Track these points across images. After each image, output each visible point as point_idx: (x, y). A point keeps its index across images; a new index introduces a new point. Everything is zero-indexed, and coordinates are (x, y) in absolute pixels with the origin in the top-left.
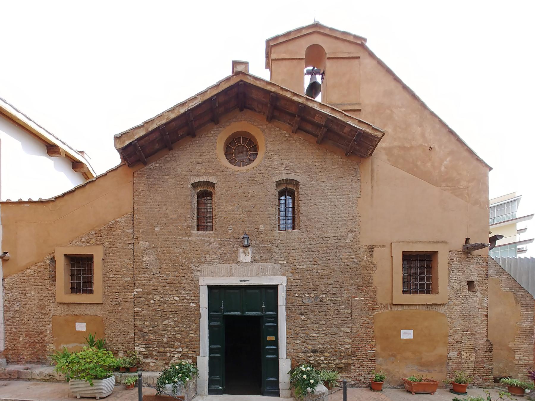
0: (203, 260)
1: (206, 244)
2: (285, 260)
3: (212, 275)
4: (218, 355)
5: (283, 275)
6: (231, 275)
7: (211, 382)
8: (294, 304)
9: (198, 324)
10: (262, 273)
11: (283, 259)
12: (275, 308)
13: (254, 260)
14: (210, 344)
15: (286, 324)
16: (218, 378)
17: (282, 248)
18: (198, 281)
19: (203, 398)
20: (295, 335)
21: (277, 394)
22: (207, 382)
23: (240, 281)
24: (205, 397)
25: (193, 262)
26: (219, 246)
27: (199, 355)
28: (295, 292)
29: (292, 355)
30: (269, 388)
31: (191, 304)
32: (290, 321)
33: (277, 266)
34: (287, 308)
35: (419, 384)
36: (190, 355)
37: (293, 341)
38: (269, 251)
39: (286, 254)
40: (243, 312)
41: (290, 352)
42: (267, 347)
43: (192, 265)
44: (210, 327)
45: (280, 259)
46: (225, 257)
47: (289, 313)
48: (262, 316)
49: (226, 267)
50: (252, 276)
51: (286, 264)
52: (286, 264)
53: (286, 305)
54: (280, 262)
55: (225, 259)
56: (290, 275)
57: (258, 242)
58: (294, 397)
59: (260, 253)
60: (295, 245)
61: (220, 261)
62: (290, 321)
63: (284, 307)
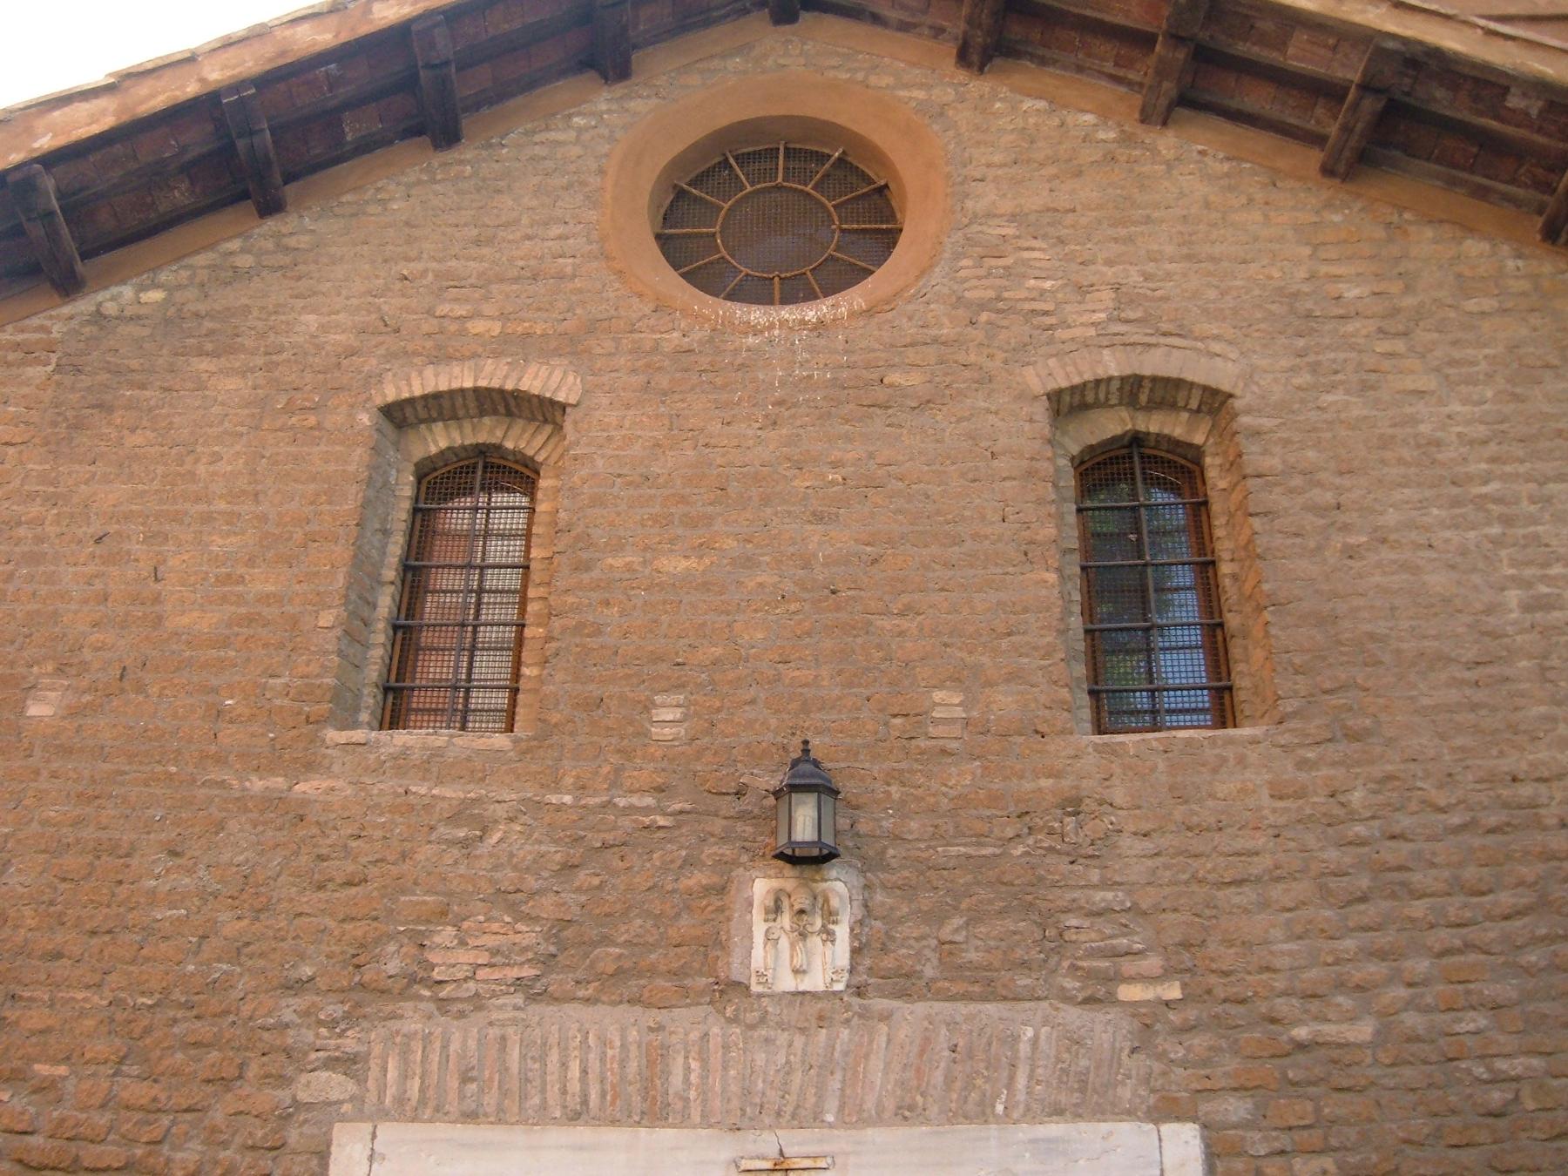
5: (1165, 1110)
11: (1153, 963)
13: (880, 973)
17: (1137, 871)
25: (297, 987)
26: (556, 854)
33: (1105, 1030)
43: (288, 1010)
46: (606, 940)
51: (1192, 1014)
52: (1192, 1014)
54: (1130, 992)
56: (1236, 1108)
59: (936, 917)
60: (1260, 841)
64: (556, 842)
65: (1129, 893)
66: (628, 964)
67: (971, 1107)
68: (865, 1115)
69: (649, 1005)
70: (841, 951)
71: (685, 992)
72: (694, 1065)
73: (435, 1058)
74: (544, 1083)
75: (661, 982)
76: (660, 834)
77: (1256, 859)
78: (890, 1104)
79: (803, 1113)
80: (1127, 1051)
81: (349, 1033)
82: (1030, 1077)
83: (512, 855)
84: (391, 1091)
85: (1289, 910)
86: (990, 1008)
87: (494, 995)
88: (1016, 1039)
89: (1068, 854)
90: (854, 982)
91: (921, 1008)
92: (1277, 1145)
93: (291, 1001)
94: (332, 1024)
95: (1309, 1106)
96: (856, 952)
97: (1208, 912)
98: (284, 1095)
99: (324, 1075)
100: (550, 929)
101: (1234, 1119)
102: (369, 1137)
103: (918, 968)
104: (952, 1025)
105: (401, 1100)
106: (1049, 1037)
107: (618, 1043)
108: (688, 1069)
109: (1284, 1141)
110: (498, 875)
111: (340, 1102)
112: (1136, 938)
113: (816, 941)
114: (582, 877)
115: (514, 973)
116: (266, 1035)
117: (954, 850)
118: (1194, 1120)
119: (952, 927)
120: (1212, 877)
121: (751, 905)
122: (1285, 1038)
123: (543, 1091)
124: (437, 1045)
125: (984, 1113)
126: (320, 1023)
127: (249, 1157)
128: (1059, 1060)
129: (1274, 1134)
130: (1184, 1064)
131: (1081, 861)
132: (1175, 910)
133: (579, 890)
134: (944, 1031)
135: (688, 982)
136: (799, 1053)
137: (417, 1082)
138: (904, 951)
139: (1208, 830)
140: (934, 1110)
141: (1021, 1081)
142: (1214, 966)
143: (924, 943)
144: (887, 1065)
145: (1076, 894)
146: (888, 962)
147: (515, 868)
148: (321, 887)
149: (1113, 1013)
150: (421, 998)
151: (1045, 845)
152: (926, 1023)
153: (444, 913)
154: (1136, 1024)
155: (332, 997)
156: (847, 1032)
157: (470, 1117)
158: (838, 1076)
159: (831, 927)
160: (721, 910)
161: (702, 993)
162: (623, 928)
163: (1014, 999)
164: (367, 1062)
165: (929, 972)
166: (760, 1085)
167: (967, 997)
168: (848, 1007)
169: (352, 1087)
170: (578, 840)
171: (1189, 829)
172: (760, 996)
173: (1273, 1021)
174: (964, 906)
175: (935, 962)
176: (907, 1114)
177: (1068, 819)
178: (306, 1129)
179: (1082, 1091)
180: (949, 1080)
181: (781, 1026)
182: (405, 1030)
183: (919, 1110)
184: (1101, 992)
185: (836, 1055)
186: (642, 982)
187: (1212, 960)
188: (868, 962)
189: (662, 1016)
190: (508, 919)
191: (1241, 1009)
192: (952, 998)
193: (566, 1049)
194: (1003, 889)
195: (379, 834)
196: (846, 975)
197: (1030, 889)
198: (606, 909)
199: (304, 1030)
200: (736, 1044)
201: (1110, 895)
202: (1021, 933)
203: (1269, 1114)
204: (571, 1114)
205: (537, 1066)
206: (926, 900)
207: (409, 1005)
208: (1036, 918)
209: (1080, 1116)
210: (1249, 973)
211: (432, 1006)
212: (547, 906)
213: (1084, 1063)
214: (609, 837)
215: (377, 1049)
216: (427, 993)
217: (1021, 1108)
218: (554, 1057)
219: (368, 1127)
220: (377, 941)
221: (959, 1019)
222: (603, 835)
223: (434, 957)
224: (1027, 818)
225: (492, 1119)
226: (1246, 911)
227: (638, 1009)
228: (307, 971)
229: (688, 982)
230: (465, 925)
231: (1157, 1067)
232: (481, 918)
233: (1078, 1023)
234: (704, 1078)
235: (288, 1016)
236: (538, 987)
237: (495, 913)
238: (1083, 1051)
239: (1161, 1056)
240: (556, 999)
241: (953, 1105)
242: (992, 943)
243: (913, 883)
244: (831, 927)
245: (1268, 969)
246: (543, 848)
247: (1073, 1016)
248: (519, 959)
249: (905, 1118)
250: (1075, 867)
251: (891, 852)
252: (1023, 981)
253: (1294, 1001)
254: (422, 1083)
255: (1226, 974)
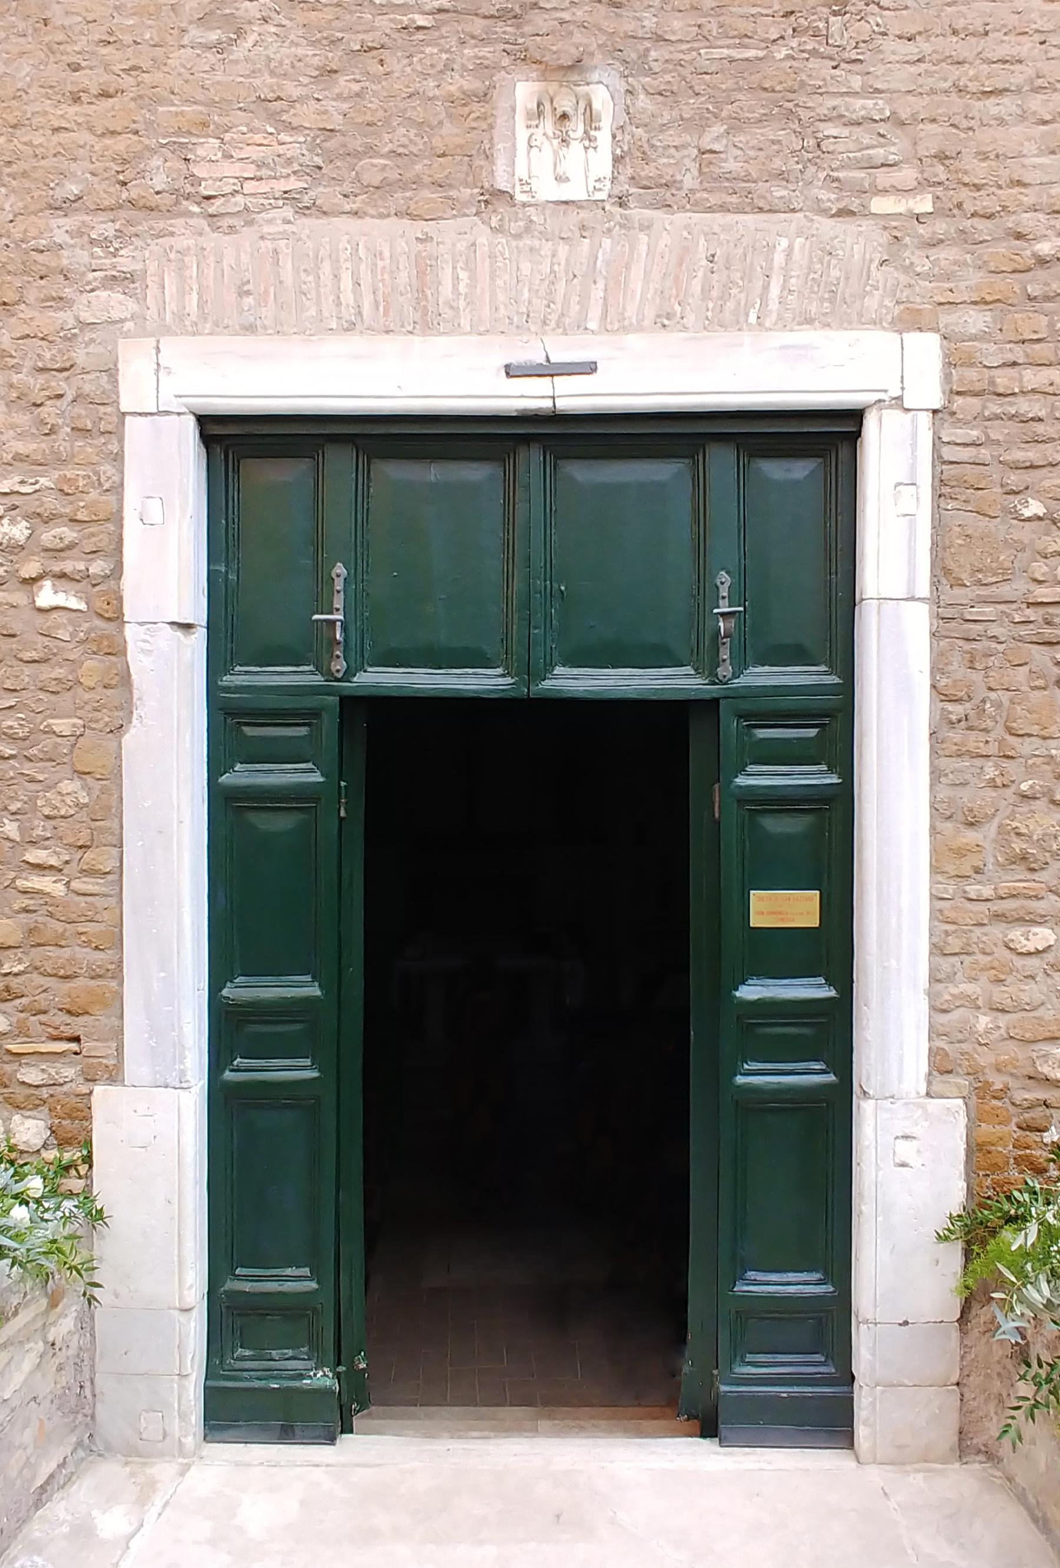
0: (159, 175)
1: (195, 34)
2: (925, 184)
3: (246, 314)
4: (300, 1070)
5: (910, 320)
6: (427, 320)
7: (231, 1320)
8: (1005, 591)
9: (107, 780)
10: (726, 309)
11: (907, 175)
12: (831, 628)
13: (642, 183)
14: (223, 963)
15: (936, 775)
16: (296, 1281)
17: (900, 78)
18: (112, 372)
19: (147, 1491)
20: (1016, 880)
21: (827, 1420)
22: (194, 1330)
23: (510, 372)
24: (164, 1471)
25: (63, 207)
26: (314, 57)
27: (114, 1075)
28: (1014, 479)
29: (985, 1059)
30: (755, 1373)
31: (47, 595)
32: (974, 742)
33: (859, 242)
34: (950, 627)
35: (345, 647)
36: (31, 1075)
37: (996, 931)
38: (785, 104)
39: (932, 138)
40: (531, 672)
41: (967, 1033)
42: (750, 992)
43: (60, 228)
44: (227, 808)
45: (883, 178)
46: (370, 151)
47: (957, 667)
48: (711, 705)
49: (371, 244)
50: (616, 324)
51: (941, 227)
52: (941, 227)
53: (935, 600)
54: (880, 205)
55: (373, 169)
56: (976, 320)
57: (678, 26)
58: (990, 1456)
59: (698, 124)
60: (1026, 47)
61: (324, 194)
62: (974, 742)
63: (918, 620)
64: (313, 44)
65: (889, 101)
66: (393, 175)
67: (727, 315)
68: (626, 323)
69: (413, 217)
70: (602, 162)
71: (453, 203)
72: (463, 275)
73: (210, 273)
74: (319, 296)
75: (426, 194)
76: (420, 36)
77: (1018, 67)
78: (650, 314)
79: (567, 321)
80: (876, 263)
81: (122, 252)
82: (783, 288)
83: (269, 60)
84: (171, 307)
85: (1045, 123)
86: (750, 219)
87: (263, 209)
88: (771, 248)
89: (832, 59)
90: (616, 192)
91: (681, 218)
92: (1010, 357)
93: (62, 221)
94: (104, 242)
95: (1044, 320)
96: (617, 160)
97: (965, 124)
98: (66, 317)
99: (103, 294)
100: (314, 139)
101: (973, 331)
102: (154, 352)
103: (678, 177)
104: (710, 235)
105: (181, 316)
106: (802, 247)
107: (387, 254)
108: (456, 279)
109: (1018, 353)
110: (256, 82)
111: (122, 321)
112: (893, 149)
113: (576, 147)
114: (343, 83)
115: (282, 185)
116: (40, 258)
117: (717, 53)
118: (936, 330)
119: (713, 136)
120: (973, 87)
121: (514, 110)
122: (1028, 253)
123: (318, 303)
124: (211, 260)
125: (738, 322)
126: (92, 242)
127: (42, 379)
128: (810, 270)
129: (1008, 346)
130: (929, 277)
131: (843, 65)
132: (934, 120)
133: (339, 97)
134: (702, 241)
135: (453, 193)
136: (563, 263)
137: (195, 296)
138: (665, 160)
139: (973, 34)
140: (690, 319)
141: (775, 291)
142: (966, 180)
143: (685, 152)
144: (647, 273)
145: (832, 102)
146: (650, 171)
147: (272, 73)
148: (77, 100)
149: (866, 225)
150: (192, 214)
151: (809, 47)
152: (685, 234)
153: (205, 125)
154: (885, 238)
155: (103, 216)
156: (609, 241)
157: (250, 329)
158: (601, 285)
159: (592, 133)
160: (483, 118)
161: (467, 204)
162: (387, 137)
163: (770, 211)
164: (144, 279)
165: (689, 181)
166: (526, 294)
167: (724, 208)
168: (610, 217)
169: (132, 306)
170: (335, 42)
171: (955, 32)
172: (524, 205)
173: (1019, 236)
174: (724, 114)
175: (696, 173)
176: (666, 322)
177: (832, 19)
178: (91, 349)
179: (831, 301)
180: (706, 291)
181: (545, 236)
182: (178, 246)
183: (678, 319)
184: (855, 205)
185: (599, 263)
186: (408, 194)
187: (966, 173)
188: (629, 172)
189: (429, 227)
190: (271, 130)
191: (988, 223)
192: (710, 210)
193: (338, 261)
194: (766, 95)
195: (128, 39)
196: (608, 183)
197: (791, 96)
198: (368, 118)
199: (78, 251)
200: (502, 254)
201: (870, 103)
202: (779, 142)
203: (1005, 328)
204: (346, 325)
205: (310, 278)
206: (690, 106)
207: (180, 222)
208: (795, 126)
209: (829, 325)
210: (1000, 187)
211: (203, 223)
212: (306, 115)
213: (835, 273)
214: (369, 39)
215: (152, 267)
216: (195, 209)
217: (774, 316)
218: (326, 268)
219: (152, 341)
220: (138, 156)
221: (716, 229)
222: (361, 36)
223: (199, 171)
224: (792, 18)
225: (270, 331)
226: (1002, 122)
227: (406, 222)
228: (74, 189)
229: (453, 193)
230: (227, 137)
231: (903, 279)
232: (244, 129)
233: (832, 234)
234: (472, 286)
235: (60, 237)
236: (306, 200)
237: (256, 123)
238: (834, 262)
239: (908, 269)
240: (325, 213)
241: (709, 314)
242: (752, 153)
243: (675, 88)
244: (592, 133)
245: (1020, 183)
246: (300, 51)
247: (827, 226)
248: (285, 171)
249: (664, 326)
250: (837, 72)
251: (653, 54)
252: (779, 192)
253: (1041, 216)
254: (200, 298)
255: (978, 187)
